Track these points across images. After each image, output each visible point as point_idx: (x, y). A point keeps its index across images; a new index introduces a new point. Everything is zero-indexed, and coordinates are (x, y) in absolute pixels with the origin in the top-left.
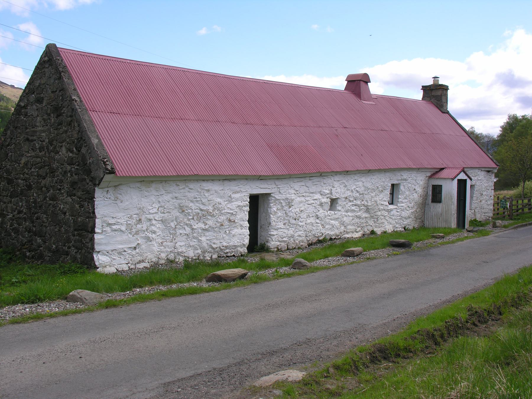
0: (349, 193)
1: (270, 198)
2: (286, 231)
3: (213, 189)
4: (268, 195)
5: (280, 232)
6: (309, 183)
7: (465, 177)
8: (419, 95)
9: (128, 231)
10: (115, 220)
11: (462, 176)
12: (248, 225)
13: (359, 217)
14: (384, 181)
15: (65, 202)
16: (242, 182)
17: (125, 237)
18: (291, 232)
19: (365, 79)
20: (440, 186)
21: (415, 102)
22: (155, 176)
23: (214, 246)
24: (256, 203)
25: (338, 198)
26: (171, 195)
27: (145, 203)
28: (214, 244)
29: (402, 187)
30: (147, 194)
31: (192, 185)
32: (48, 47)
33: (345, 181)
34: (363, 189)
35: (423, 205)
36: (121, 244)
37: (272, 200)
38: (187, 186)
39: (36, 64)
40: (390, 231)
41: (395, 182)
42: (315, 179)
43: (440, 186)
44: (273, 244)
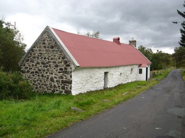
0: (124, 71)
4: (108, 72)
6: (116, 69)
9: (81, 83)
13: (125, 78)
14: (129, 68)
16: (104, 69)
19: (119, 39)
20: (142, 69)
21: (111, 42)
22: (84, 67)
24: (106, 73)
31: (93, 70)
36: (78, 87)
37: (108, 74)
39: (40, 34)
40: (73, 95)
41: (132, 68)
42: (117, 68)
43: (142, 69)
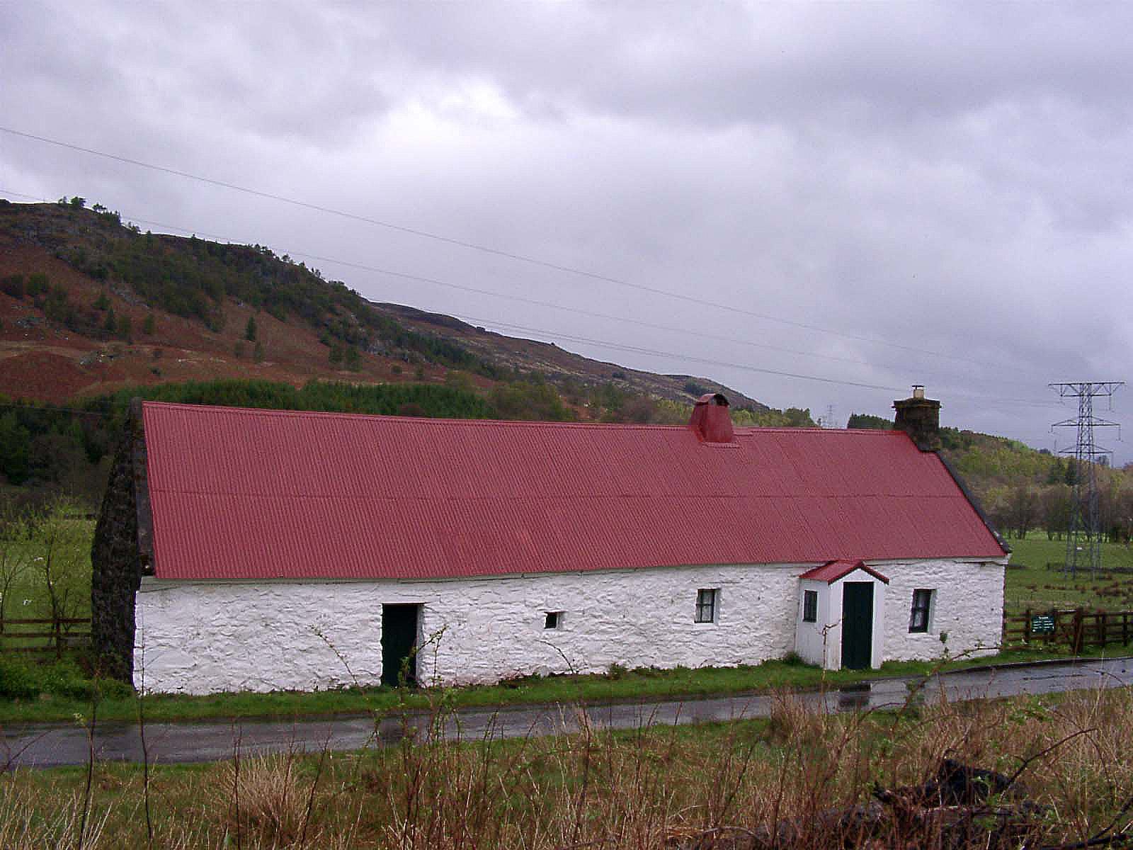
1: (425, 610)
2: (455, 660)
3: (314, 595)
5: (440, 662)
7: (868, 578)
8: (891, 416)
10: (162, 632)
11: (858, 576)
12: (381, 647)
14: (688, 584)
15: (127, 609)
17: (176, 654)
18: (462, 660)
20: (815, 593)
23: (320, 674)
25: (563, 612)
26: (246, 603)
27: (205, 612)
28: (319, 670)
29: (724, 595)
30: (208, 600)
32: (938, 403)
33: (578, 586)
34: (623, 596)
35: (788, 625)
38: (271, 592)
43: (815, 593)
44: (426, 676)
